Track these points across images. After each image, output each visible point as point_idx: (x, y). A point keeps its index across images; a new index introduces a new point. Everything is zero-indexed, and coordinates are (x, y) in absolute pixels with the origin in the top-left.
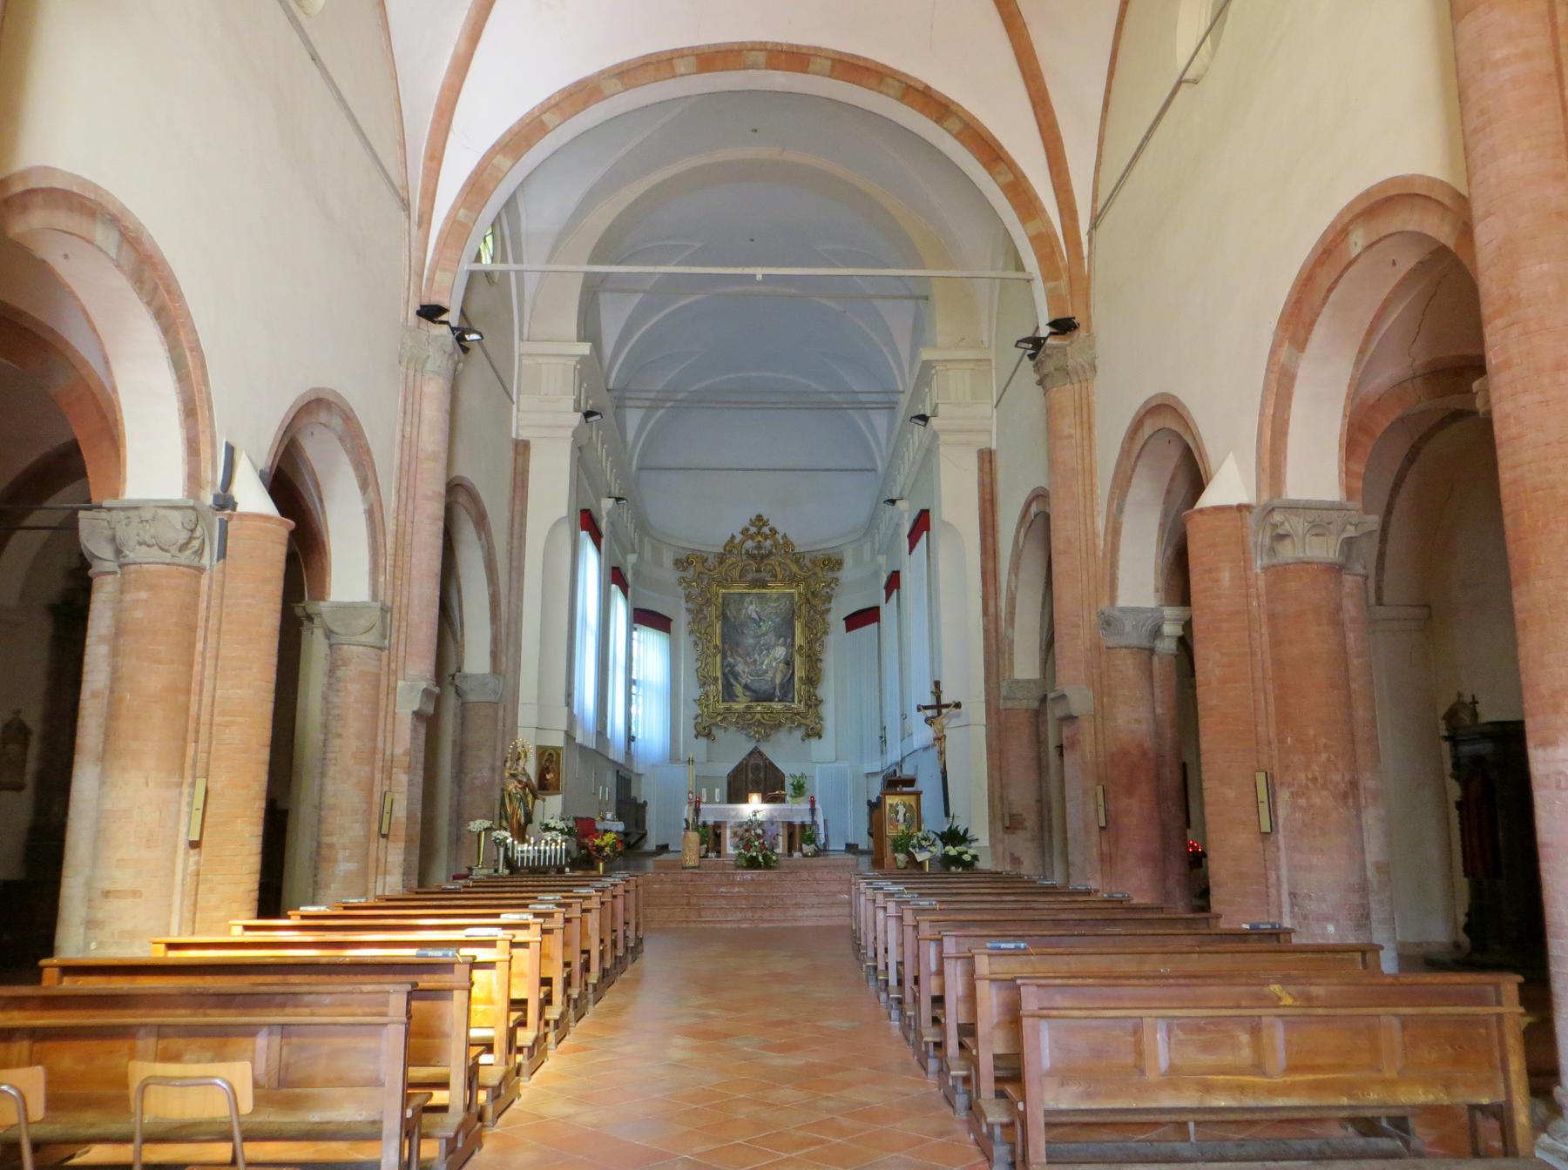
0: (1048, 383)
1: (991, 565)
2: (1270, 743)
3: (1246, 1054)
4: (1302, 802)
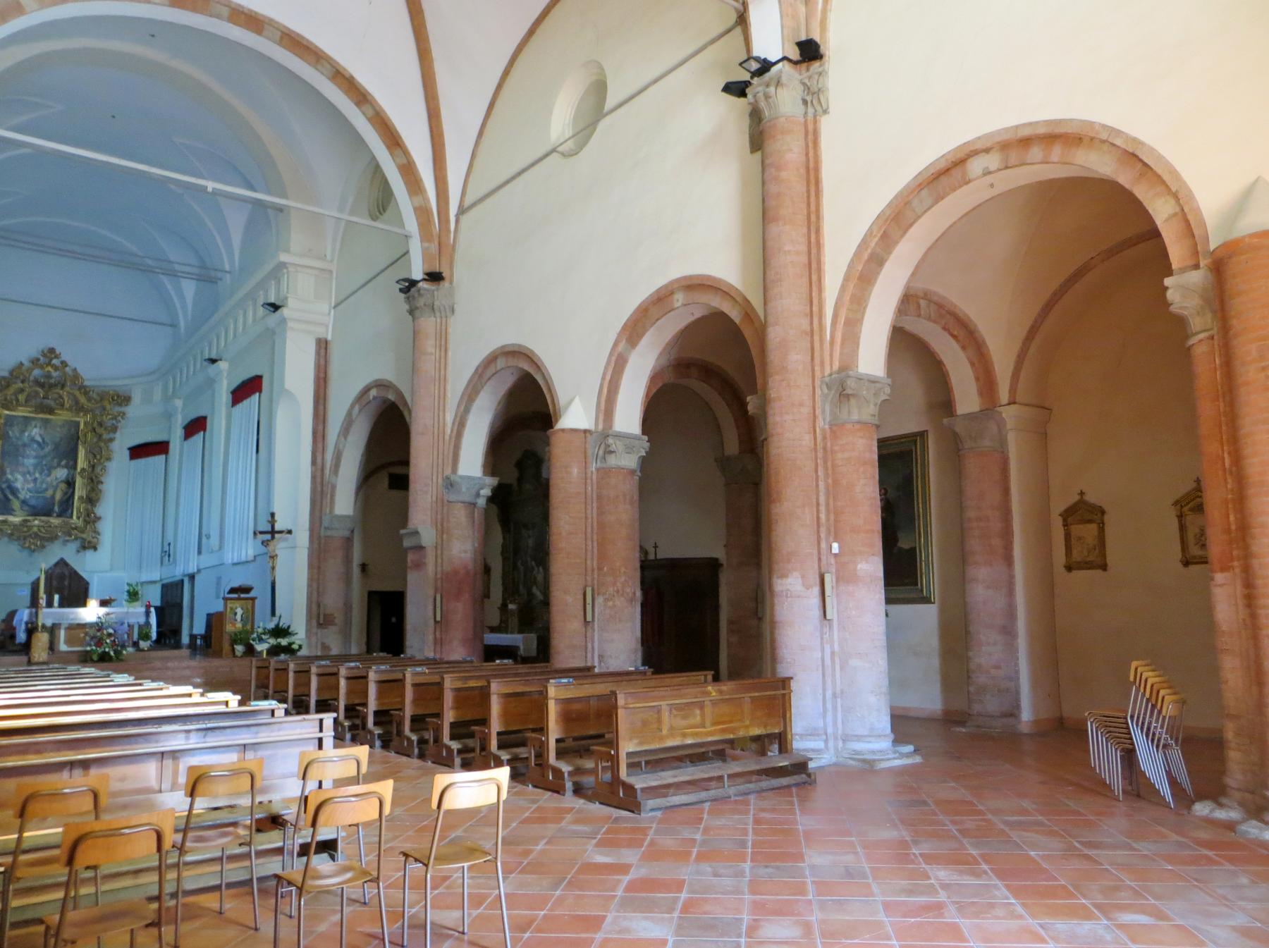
0: (417, 313)
1: (321, 427)
3: (698, 718)
4: (610, 604)
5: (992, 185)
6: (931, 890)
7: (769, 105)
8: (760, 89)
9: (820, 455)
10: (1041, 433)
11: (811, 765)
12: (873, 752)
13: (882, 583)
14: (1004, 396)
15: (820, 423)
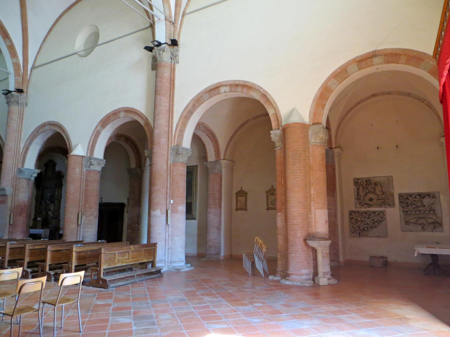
0: (11, 104)
2: (82, 206)
4: (88, 218)
5: (226, 96)
6: (205, 303)
7: (160, 58)
8: (157, 51)
9: (169, 172)
10: (231, 170)
11: (162, 271)
12: (180, 266)
13: (185, 213)
14: (222, 156)
15: (169, 161)
